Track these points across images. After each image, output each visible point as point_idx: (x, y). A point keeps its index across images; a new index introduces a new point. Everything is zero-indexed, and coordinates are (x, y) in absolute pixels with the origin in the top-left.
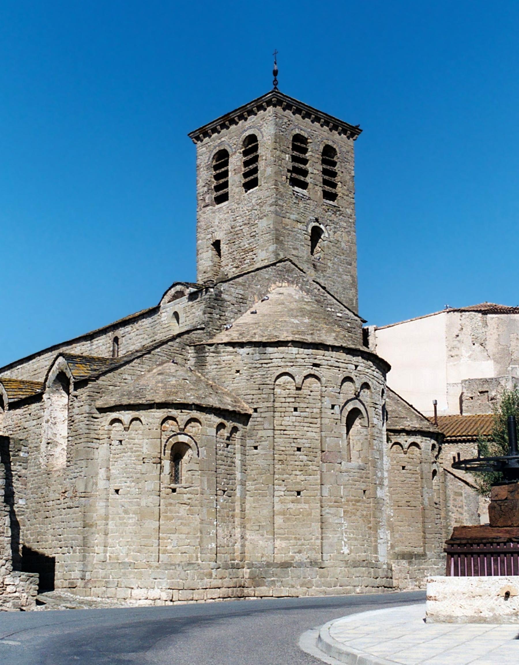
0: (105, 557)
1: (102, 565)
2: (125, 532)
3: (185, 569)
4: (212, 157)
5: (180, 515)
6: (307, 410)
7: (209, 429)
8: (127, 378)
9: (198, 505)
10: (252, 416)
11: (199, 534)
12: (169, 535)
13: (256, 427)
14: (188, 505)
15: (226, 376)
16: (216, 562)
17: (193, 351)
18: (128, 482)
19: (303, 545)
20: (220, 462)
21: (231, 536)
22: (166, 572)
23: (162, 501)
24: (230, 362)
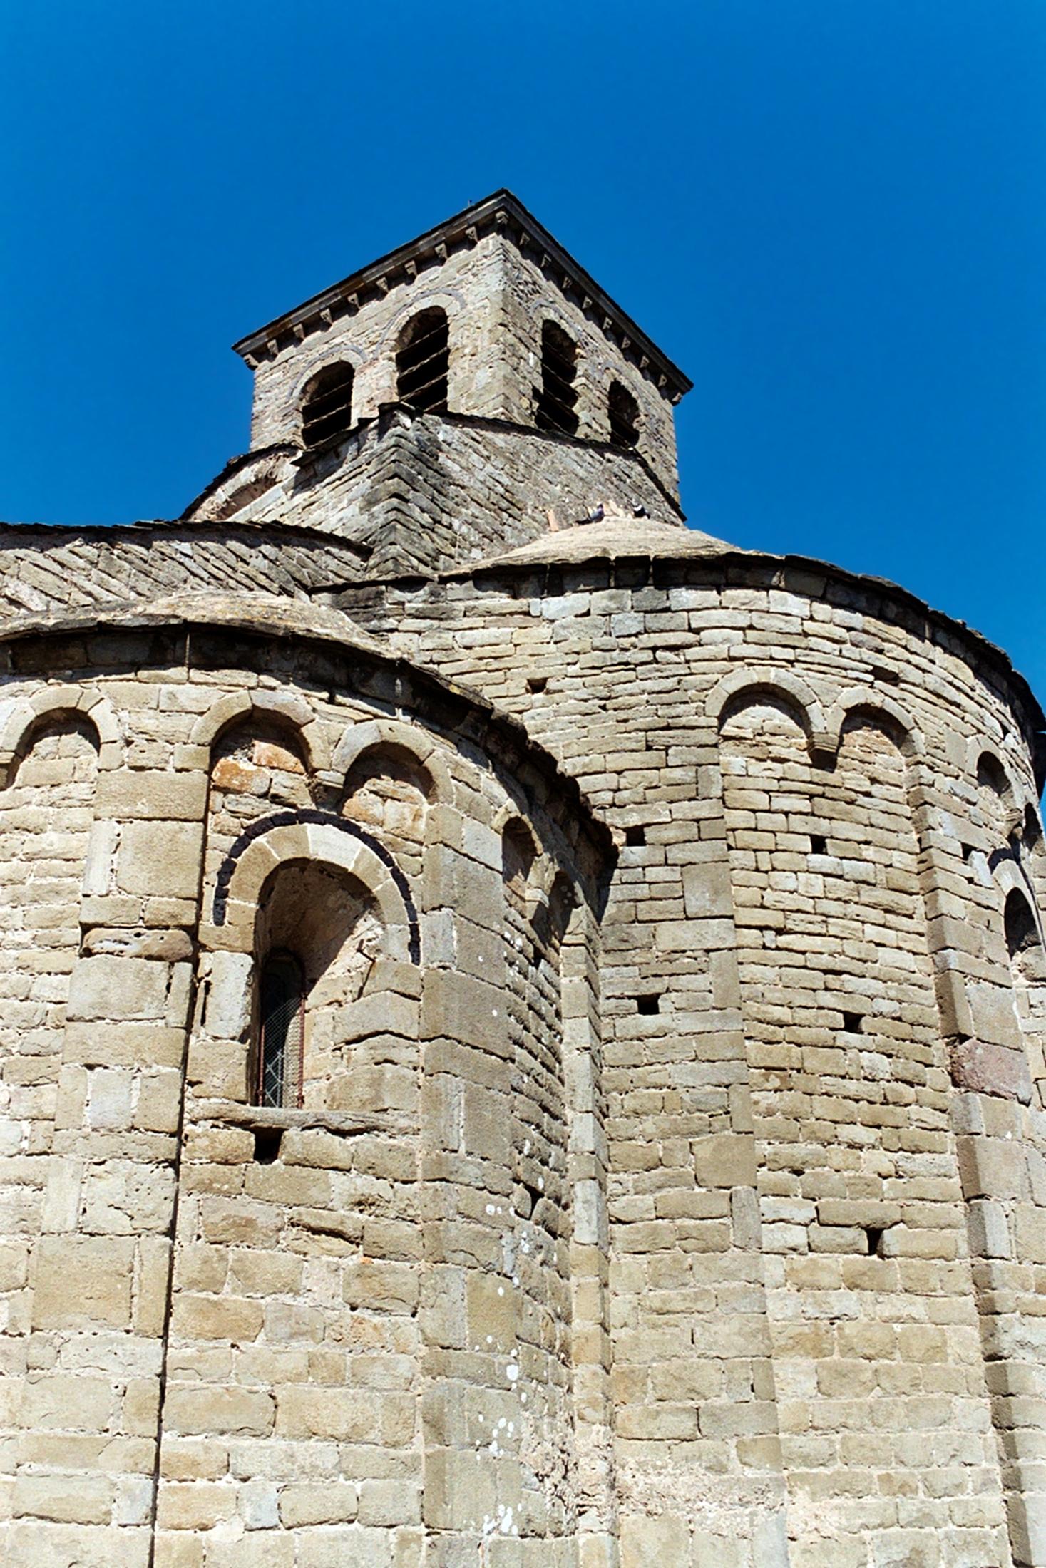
4: (300, 386)
5: (302, 1302)
6: (868, 852)
7: (470, 828)
9: (417, 1250)
10: (621, 861)
11: (419, 1446)
12: (225, 1441)
14: (355, 1241)
19: (924, 1519)
23: (188, 1205)
24: (498, 651)
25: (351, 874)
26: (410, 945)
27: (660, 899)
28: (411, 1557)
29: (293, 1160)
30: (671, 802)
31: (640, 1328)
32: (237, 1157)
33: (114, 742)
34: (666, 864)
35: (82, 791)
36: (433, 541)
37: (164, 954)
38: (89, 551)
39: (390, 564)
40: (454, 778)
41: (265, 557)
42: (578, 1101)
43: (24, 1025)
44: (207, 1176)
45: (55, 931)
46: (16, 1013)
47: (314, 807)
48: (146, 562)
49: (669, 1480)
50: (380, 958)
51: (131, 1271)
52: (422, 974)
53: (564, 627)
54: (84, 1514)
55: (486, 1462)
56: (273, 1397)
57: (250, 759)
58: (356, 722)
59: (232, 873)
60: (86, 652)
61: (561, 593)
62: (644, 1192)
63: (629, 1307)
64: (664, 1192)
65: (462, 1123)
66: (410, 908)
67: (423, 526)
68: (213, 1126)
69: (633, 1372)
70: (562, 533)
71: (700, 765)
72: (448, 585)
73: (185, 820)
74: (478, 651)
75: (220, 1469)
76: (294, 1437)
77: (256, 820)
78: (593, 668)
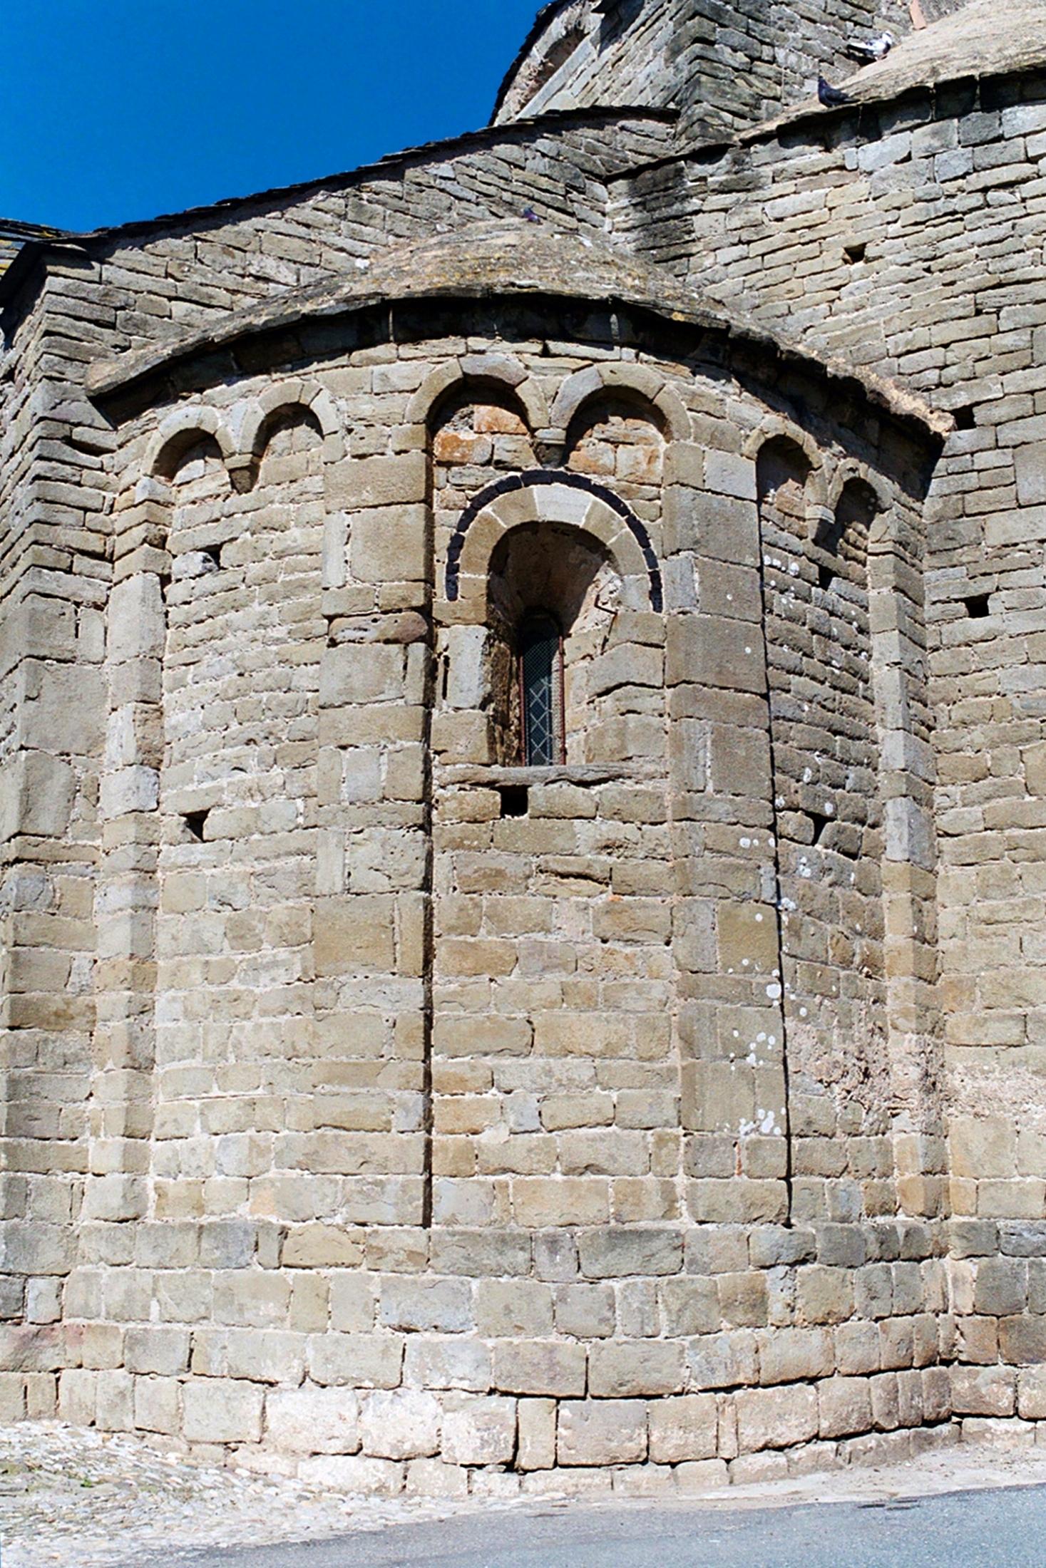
0: (133, 1194)
1: (111, 1240)
2: (238, 1045)
3: (596, 1270)
7: (713, 461)
8: (271, 272)
9: (668, 885)
10: (946, 450)
11: (676, 1059)
12: (488, 1060)
13: (973, 503)
15: (793, 284)
16: (788, 1225)
17: (624, 202)
18: (252, 763)
20: (784, 654)
21: (866, 1074)
22: (475, 1284)
25: (583, 531)
26: (651, 593)
27: (990, 488)
28: (668, 1155)
29: (538, 814)
30: (1004, 374)
31: (968, 939)
32: (484, 815)
33: (335, 432)
34: (998, 447)
35: (315, 484)
36: (751, 85)
37: (400, 637)
38: (335, 202)
39: (696, 128)
40: (690, 410)
41: (544, 155)
42: (889, 718)
43: (290, 714)
44: (457, 835)
45: (307, 624)
46: (281, 704)
47: (539, 467)
48: (401, 199)
49: (996, 1084)
50: (621, 610)
51: (392, 922)
52: (665, 620)
53: (883, 179)
54: (369, 1124)
55: (742, 1072)
56: (529, 1022)
57: (471, 427)
58: (574, 371)
59: (461, 547)
60: (299, 344)
61: (878, 137)
62: (972, 804)
63: (957, 918)
64: (993, 803)
65: (709, 763)
66: (650, 555)
67: (736, 70)
68: (460, 789)
69: (960, 981)
70: (932, 27)
71: (1036, 326)
72: (752, 149)
73: (408, 503)
74: (791, 222)
75: (485, 1084)
76: (551, 1055)
77: (481, 489)
78: (916, 224)
